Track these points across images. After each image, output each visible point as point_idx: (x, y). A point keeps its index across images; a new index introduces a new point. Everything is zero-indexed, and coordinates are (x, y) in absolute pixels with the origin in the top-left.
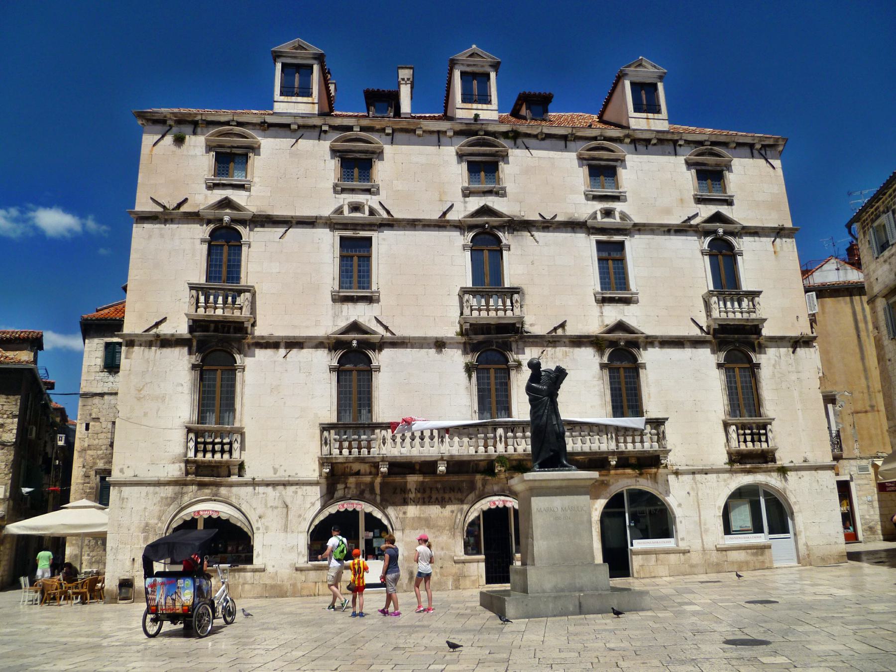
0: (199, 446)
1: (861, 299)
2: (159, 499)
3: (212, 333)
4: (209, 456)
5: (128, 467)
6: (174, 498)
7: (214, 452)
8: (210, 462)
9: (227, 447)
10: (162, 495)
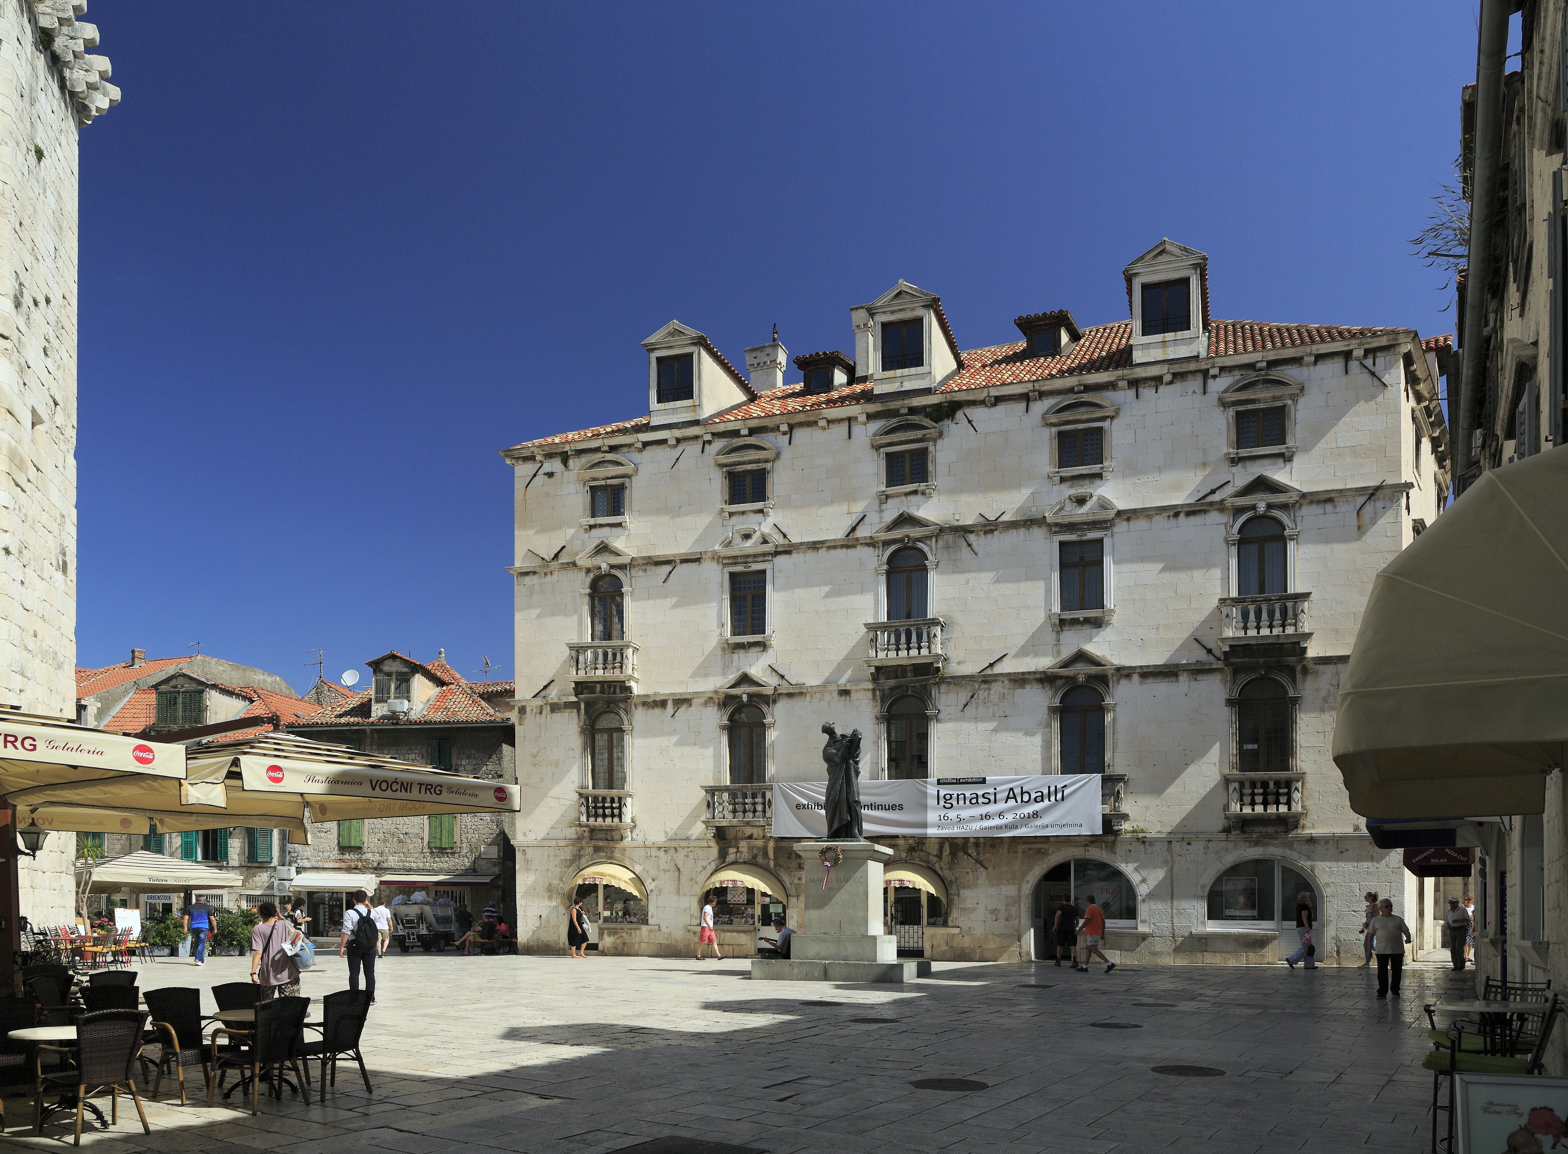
2: (559, 861)
4: (600, 820)
7: (604, 816)
9: (616, 811)
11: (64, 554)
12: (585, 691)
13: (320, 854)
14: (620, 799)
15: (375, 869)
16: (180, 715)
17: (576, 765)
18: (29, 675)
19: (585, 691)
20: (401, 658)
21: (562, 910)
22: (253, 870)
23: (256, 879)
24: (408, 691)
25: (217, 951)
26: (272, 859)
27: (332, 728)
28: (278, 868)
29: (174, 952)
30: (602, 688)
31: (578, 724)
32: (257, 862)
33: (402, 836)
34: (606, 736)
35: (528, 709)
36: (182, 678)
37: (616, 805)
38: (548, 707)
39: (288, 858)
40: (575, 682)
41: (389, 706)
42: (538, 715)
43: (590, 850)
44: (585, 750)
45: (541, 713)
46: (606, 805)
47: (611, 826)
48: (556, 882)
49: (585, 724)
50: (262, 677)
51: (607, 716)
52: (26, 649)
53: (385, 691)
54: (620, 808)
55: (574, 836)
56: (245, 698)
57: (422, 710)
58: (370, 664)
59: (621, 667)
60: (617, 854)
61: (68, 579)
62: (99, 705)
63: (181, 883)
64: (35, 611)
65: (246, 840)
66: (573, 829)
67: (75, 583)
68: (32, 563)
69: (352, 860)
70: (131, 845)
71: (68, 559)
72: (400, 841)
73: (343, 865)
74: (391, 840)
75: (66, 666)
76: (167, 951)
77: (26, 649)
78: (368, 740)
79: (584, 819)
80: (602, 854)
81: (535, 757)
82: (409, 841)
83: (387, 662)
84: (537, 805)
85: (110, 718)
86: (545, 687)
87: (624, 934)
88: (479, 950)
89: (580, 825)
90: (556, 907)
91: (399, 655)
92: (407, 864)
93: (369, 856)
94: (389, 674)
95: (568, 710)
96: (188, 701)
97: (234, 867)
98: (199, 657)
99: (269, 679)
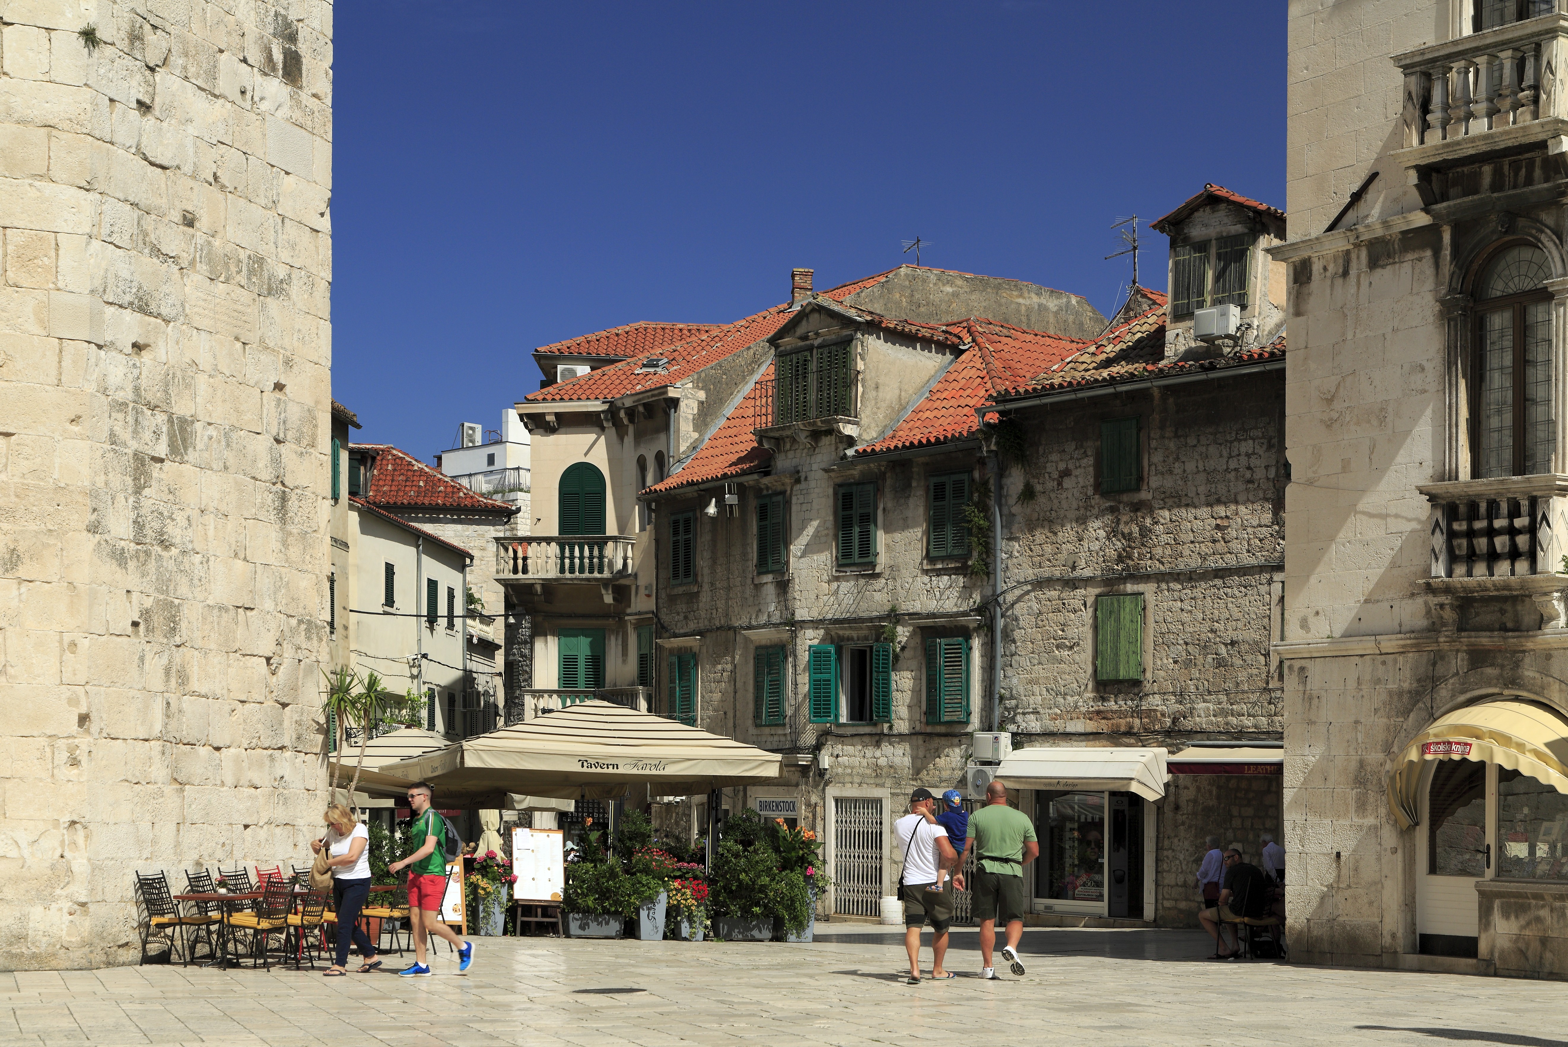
0: (1455, 542)
1: (548, 540)
2: (1384, 696)
3: (1459, 201)
4: (1480, 569)
5: (1317, 613)
6: (1418, 693)
7: (1492, 557)
8: (1483, 588)
9: (1522, 541)
10: (1390, 686)
11: (292, 38)
12: (1452, 192)
13: (1060, 700)
14: (1533, 502)
15: (1168, 733)
16: (814, 397)
17: (1429, 412)
18: (164, 311)
19: (1452, 192)
20: (1226, 200)
21: (1390, 837)
22: (936, 741)
23: (941, 762)
24: (1242, 281)
25: (723, 929)
26: (969, 714)
27: (1080, 395)
28: (979, 735)
29: (631, 930)
30: (1498, 173)
31: (1436, 291)
32: (940, 723)
33: (1223, 650)
34: (1507, 315)
35: (1317, 267)
36: (816, 316)
37: (1521, 522)
38: (1364, 254)
39: (998, 712)
40: (1418, 168)
41: (1196, 328)
42: (1339, 281)
43: (1459, 662)
44: (1450, 364)
45: (1345, 273)
46: (1498, 523)
47: (1507, 587)
48: (1375, 757)
49: (1451, 290)
50: (1035, 299)
51: (1514, 255)
52: (156, 251)
53: (1194, 289)
54: (1532, 531)
55: (1421, 622)
56: (942, 347)
57: (1279, 326)
58: (1160, 226)
59: (1536, 100)
60: (1529, 672)
61: (305, 96)
62: (702, 395)
63: (647, 772)
64: (187, 168)
65: (924, 671)
66: (1420, 601)
67: (329, 101)
68: (177, 61)
69: (1121, 714)
70: (735, 692)
71: (303, 48)
72: (1220, 663)
73: (1103, 726)
74: (1200, 659)
75: (296, 289)
76: (615, 926)
77: (156, 251)
78: (1156, 417)
79: (1439, 569)
80: (1490, 671)
81: (1330, 401)
82: (1238, 662)
83: (1200, 216)
84: (1332, 539)
85: (722, 422)
86: (1357, 197)
87: (1544, 913)
88: (1107, 948)
89: (1429, 589)
90: (1375, 830)
91: (1223, 193)
92: (1234, 720)
93: (1155, 702)
94: (1202, 247)
95: (1410, 256)
96: (825, 365)
97: (900, 735)
98: (903, 270)
99: (1053, 304)
